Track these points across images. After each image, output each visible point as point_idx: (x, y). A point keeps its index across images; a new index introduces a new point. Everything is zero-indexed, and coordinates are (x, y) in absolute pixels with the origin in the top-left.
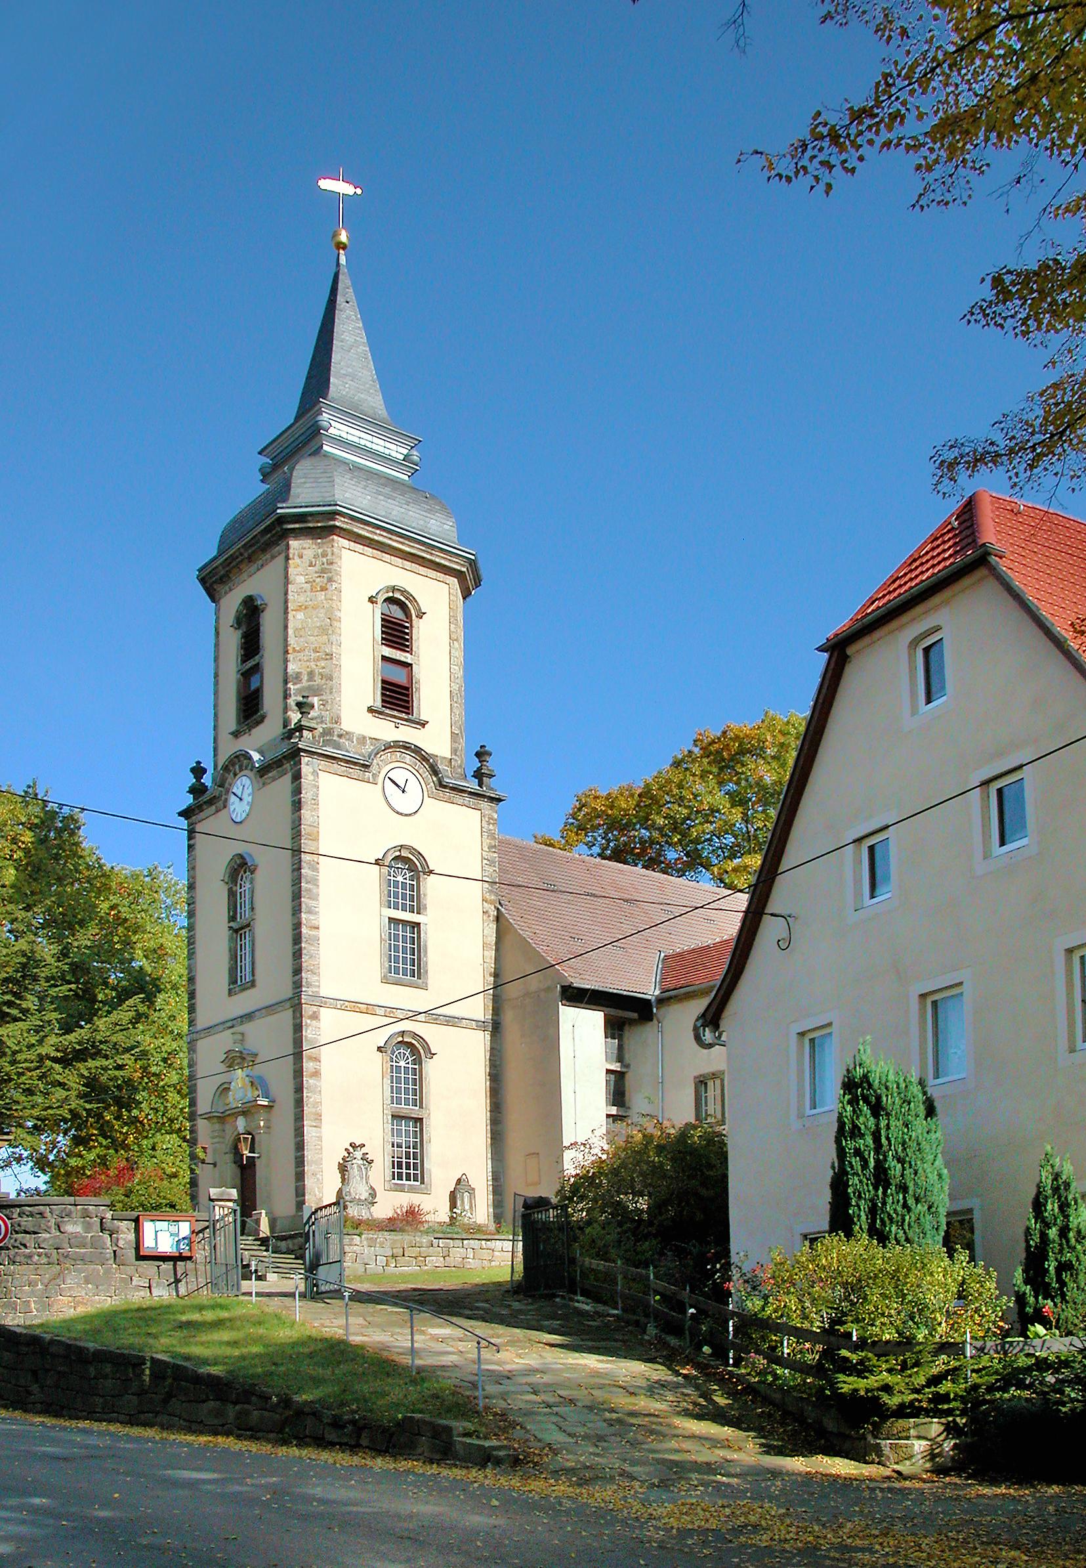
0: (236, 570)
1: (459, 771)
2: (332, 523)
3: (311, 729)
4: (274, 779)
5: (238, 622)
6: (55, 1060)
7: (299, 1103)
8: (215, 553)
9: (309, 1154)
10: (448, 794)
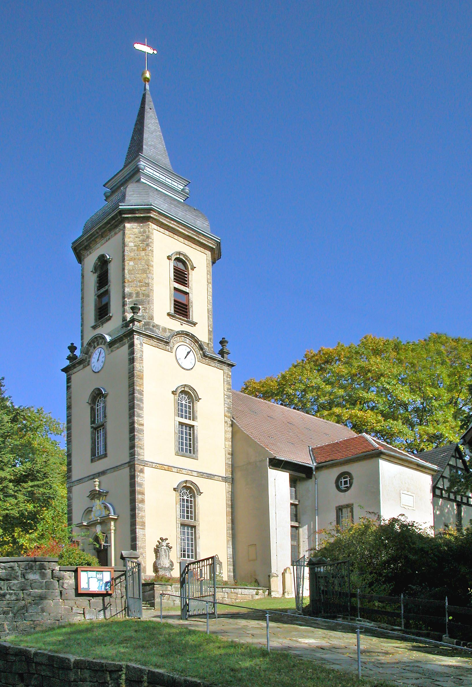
0: (93, 243)
1: (212, 350)
2: (149, 215)
3: (139, 321)
4: (118, 348)
5: (95, 270)
6: (11, 481)
7: (133, 516)
8: (81, 234)
10: (208, 361)
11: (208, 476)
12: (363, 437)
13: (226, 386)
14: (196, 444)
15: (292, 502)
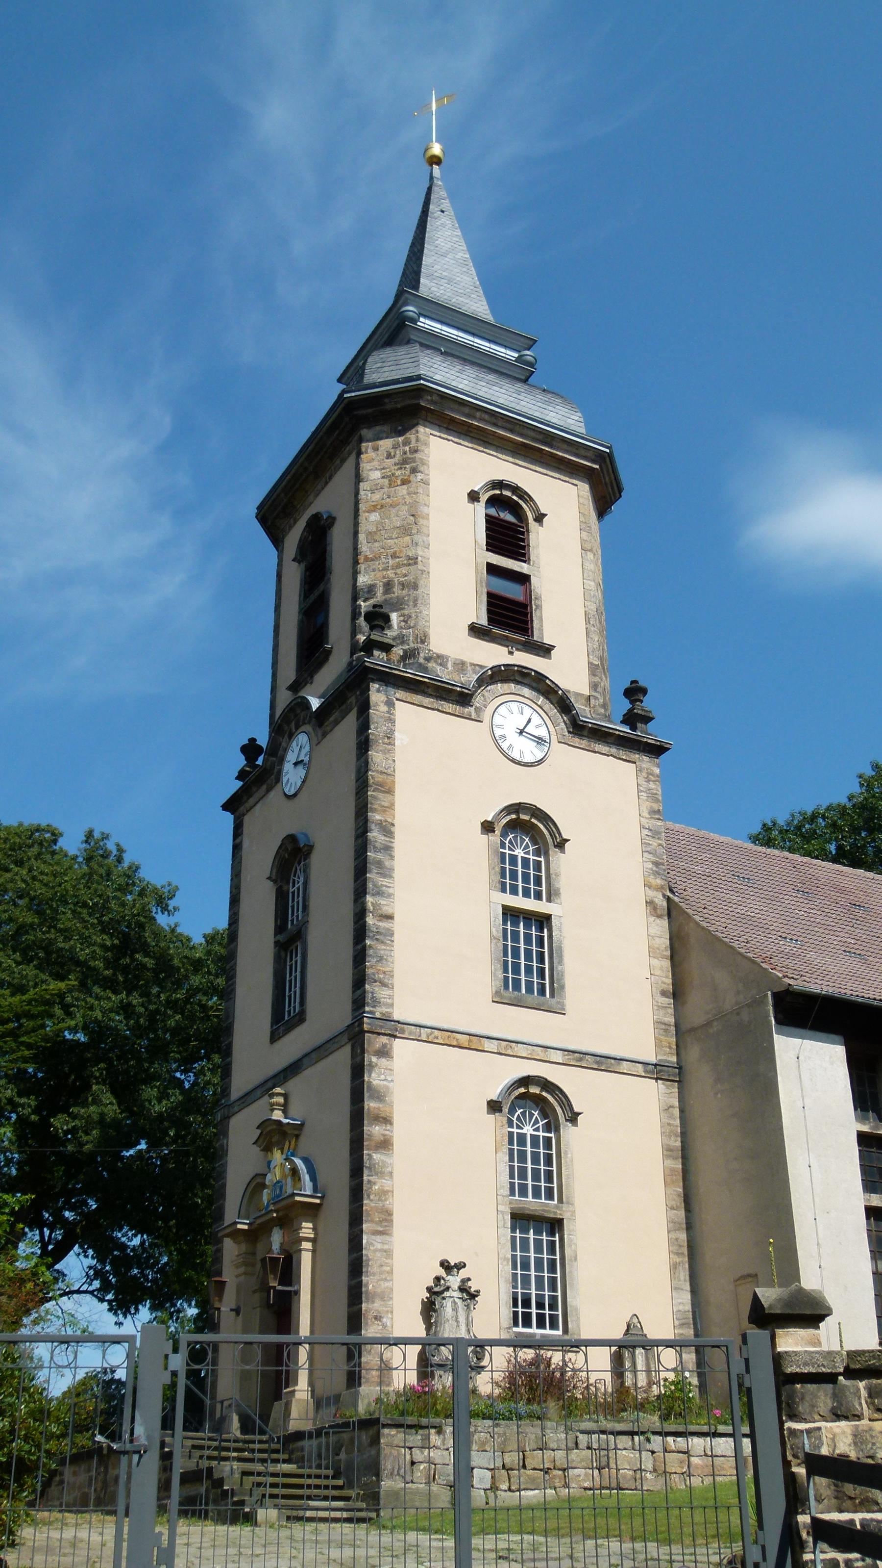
7: (357, 1193)
9: (370, 1282)
11: (597, 1063)
13: (646, 805)
14: (558, 968)
15: (865, 1128)
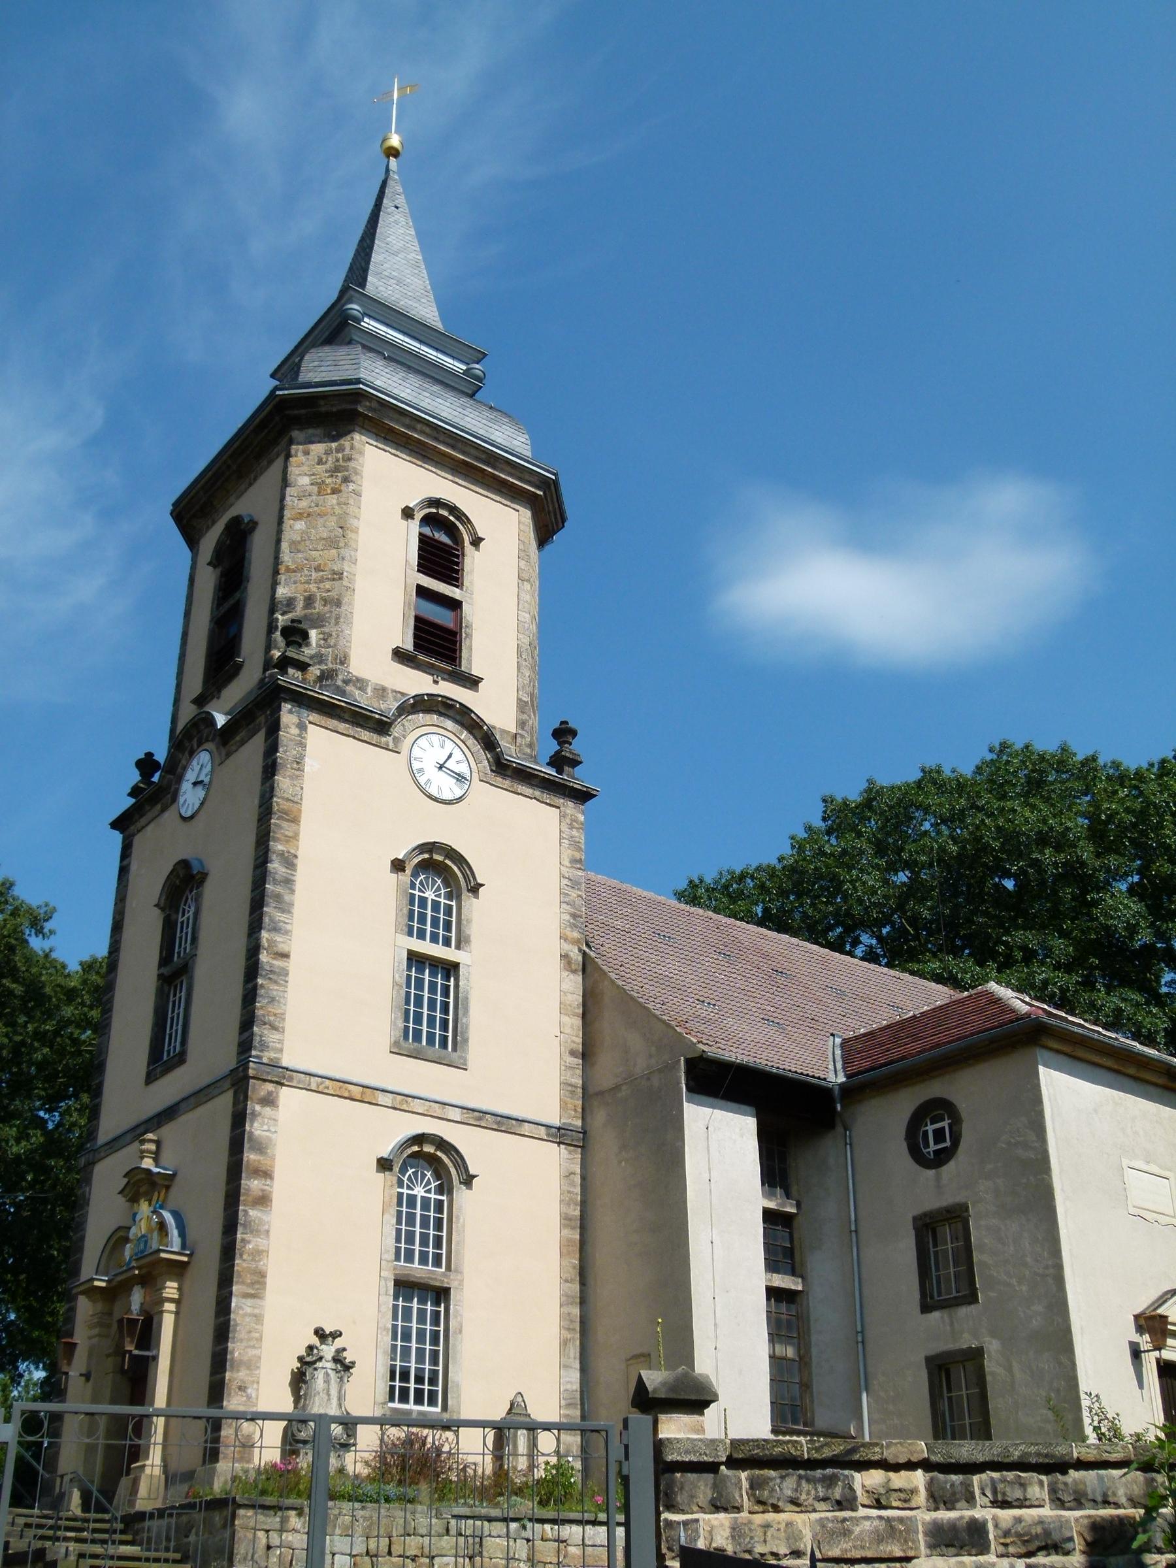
7: (228, 1252)
9: (237, 1349)
11: (498, 1123)
12: (990, 994)
13: (568, 853)
14: (462, 1020)
15: (772, 1205)
